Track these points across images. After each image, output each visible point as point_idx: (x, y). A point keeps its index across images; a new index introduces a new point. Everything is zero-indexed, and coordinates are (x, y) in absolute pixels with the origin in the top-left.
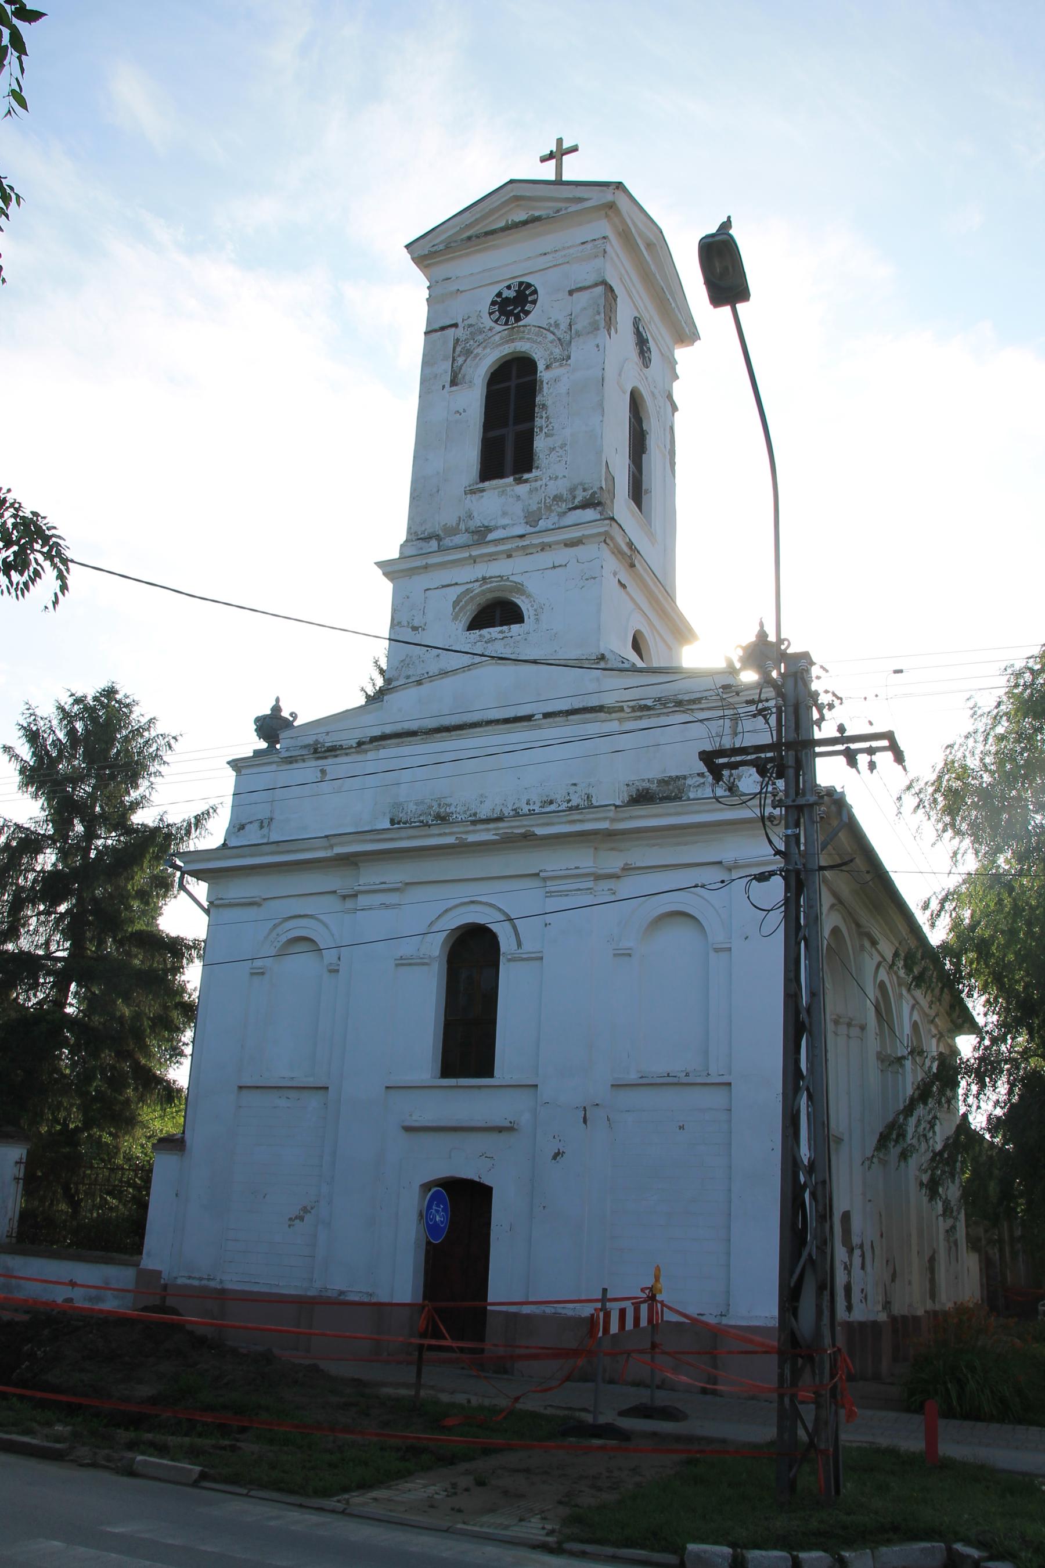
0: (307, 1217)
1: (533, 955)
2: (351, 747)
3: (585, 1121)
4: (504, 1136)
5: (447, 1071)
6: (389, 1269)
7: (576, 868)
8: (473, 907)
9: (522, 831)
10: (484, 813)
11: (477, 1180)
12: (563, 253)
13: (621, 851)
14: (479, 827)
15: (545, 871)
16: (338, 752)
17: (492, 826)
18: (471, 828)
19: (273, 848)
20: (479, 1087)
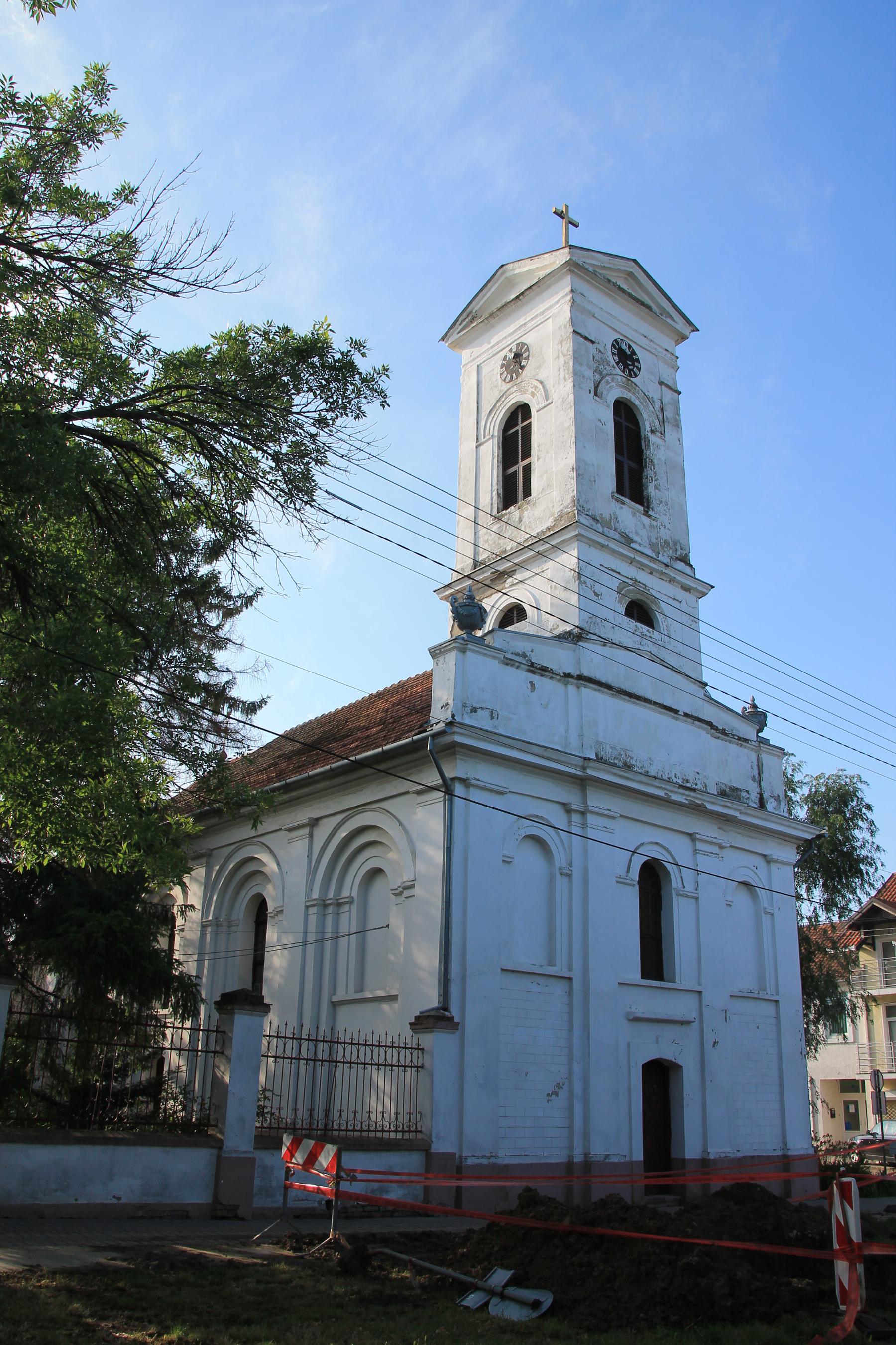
0: (561, 1092)
2: (559, 675)
4: (684, 1027)
6: (618, 1136)
10: (652, 772)
12: (654, 346)
14: (681, 791)
16: (547, 674)
17: (687, 792)
18: (676, 789)
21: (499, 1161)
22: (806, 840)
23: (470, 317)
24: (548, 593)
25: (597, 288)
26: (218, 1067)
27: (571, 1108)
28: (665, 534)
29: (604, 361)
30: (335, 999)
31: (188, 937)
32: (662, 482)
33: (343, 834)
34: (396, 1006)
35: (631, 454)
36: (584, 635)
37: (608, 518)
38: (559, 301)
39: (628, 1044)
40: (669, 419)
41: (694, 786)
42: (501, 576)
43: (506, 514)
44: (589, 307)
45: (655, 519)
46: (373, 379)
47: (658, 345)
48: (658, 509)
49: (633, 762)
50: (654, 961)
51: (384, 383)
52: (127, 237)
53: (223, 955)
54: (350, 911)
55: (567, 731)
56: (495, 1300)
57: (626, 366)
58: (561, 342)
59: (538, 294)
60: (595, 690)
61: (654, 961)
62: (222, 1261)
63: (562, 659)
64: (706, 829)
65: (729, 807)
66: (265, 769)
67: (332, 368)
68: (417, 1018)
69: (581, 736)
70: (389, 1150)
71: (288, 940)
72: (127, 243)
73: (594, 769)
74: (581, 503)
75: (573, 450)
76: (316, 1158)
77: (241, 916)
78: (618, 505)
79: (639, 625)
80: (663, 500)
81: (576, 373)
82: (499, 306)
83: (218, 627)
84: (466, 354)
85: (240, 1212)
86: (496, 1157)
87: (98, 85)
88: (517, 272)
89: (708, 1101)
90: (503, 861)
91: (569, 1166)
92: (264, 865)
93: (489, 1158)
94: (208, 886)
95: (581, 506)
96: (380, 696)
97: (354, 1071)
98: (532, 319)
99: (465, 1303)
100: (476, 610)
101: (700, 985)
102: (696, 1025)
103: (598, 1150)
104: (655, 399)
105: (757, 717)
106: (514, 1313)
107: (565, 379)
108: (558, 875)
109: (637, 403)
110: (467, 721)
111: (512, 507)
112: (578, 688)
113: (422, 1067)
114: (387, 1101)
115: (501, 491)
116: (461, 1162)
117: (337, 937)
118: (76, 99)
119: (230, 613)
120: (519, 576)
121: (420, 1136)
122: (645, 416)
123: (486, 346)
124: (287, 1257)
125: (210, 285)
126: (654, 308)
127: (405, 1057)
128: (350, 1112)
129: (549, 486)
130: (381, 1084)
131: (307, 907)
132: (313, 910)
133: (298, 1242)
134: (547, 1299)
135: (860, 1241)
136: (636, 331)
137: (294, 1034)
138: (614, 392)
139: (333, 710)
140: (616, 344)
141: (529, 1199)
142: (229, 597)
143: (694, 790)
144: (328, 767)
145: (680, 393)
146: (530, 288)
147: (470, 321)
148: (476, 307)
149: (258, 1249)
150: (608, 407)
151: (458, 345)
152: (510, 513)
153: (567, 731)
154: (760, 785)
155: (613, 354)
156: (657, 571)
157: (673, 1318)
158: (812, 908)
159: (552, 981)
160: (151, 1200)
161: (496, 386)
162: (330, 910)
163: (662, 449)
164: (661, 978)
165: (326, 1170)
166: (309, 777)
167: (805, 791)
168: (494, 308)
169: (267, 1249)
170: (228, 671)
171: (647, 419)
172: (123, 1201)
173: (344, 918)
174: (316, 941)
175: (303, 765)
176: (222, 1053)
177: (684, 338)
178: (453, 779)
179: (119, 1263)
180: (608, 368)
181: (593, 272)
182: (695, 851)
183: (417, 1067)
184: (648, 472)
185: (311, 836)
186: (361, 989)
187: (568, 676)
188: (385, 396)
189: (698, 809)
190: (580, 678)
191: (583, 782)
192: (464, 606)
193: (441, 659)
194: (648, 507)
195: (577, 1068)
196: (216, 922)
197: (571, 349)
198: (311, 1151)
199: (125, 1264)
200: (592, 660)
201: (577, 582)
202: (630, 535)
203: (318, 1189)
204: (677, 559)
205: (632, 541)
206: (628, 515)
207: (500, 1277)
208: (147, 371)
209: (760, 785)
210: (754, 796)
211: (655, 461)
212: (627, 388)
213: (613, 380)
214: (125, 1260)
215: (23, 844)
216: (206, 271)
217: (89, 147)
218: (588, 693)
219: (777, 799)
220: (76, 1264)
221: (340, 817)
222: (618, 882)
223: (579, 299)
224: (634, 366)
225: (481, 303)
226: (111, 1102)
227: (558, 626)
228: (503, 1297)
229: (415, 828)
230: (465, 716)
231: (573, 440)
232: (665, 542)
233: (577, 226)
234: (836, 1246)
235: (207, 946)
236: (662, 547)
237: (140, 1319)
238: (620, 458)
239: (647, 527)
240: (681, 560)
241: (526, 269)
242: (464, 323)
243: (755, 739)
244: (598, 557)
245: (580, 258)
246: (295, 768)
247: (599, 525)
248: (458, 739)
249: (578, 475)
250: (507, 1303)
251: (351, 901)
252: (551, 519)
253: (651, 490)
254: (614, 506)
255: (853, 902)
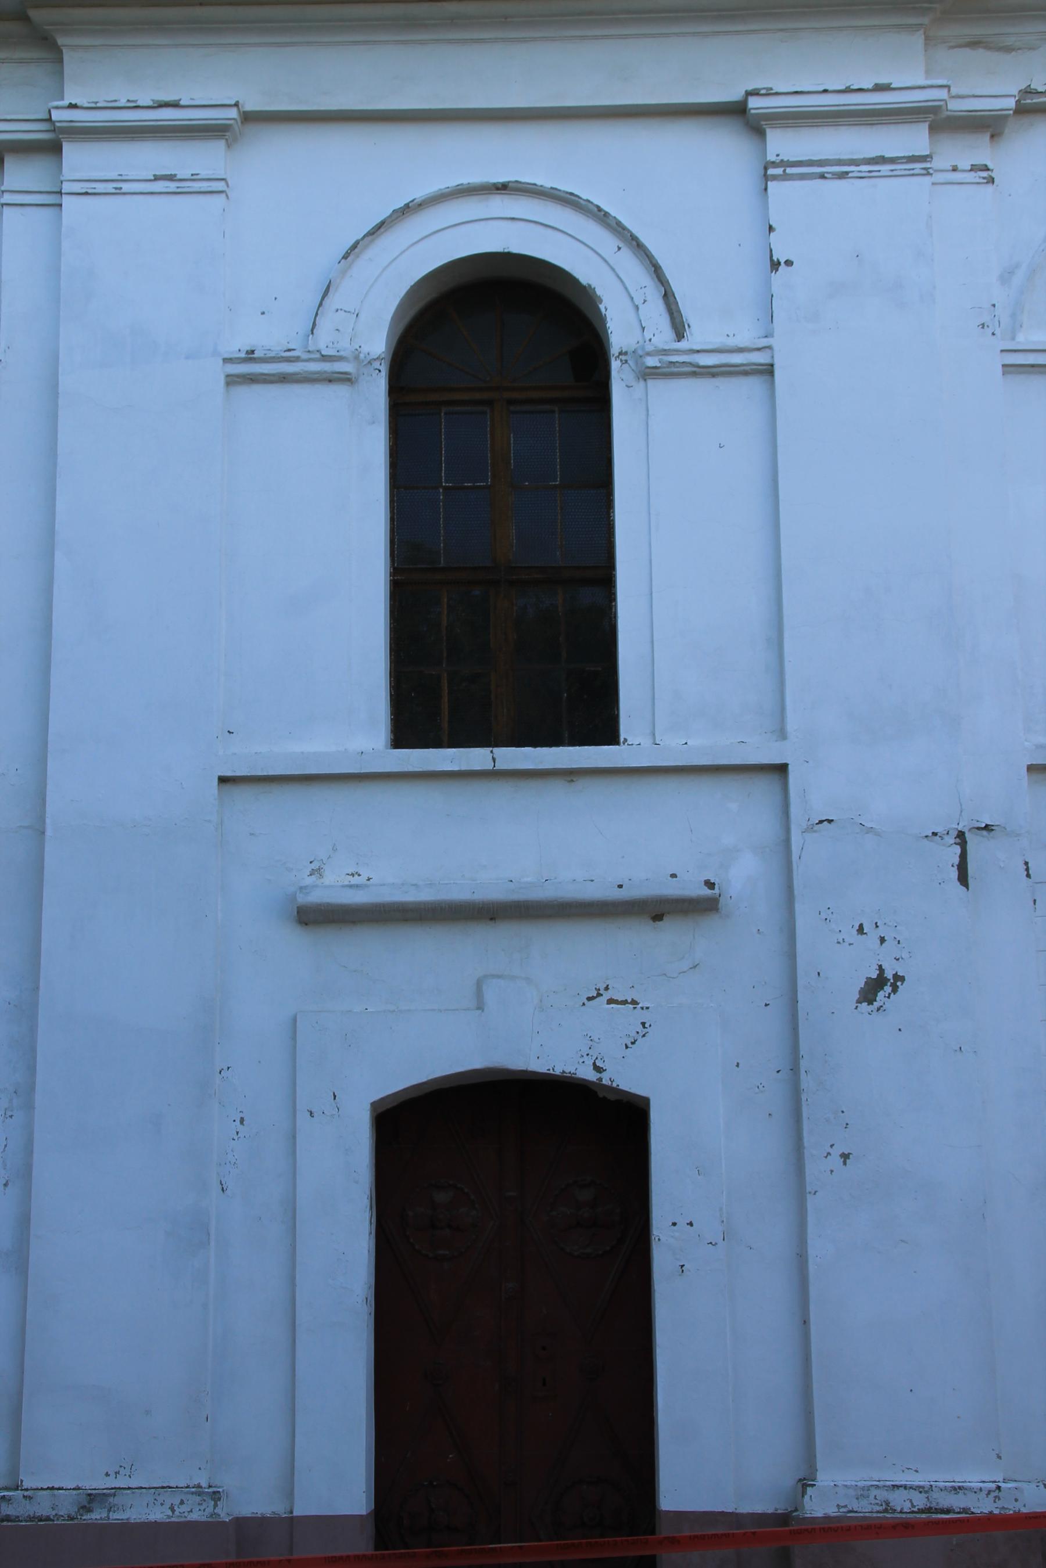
1: (737, 359)
3: (963, 878)
4: (670, 935)
5: (411, 726)
7: (879, 88)
8: (499, 205)
11: (590, 1075)
13: (1008, 49)
15: (770, 93)
20: (571, 774)
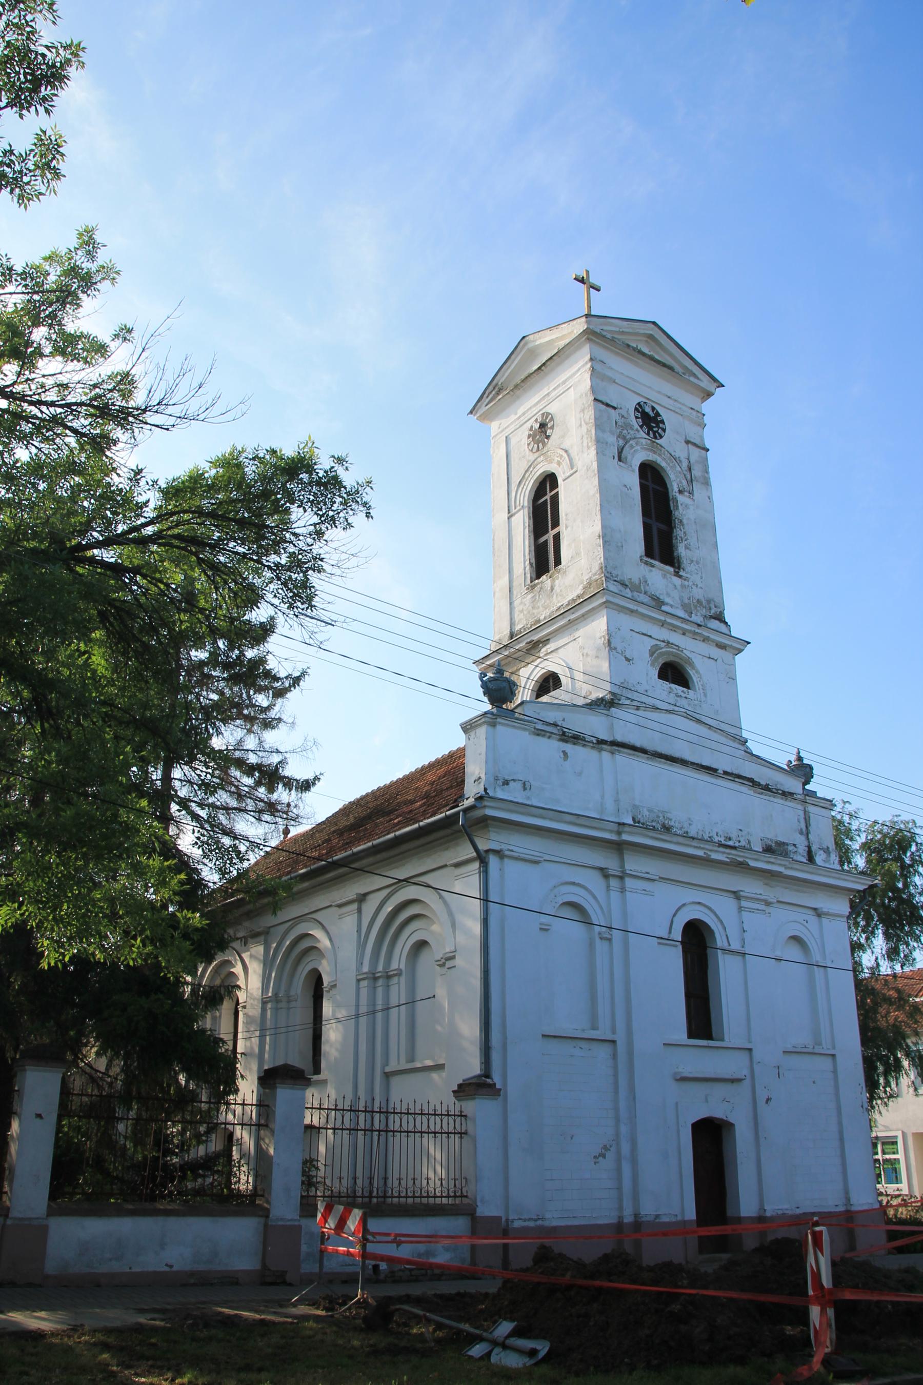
0: (608, 1154)
6: (669, 1194)
9: (741, 859)
10: (692, 833)
14: (721, 849)
17: (728, 851)
18: (716, 848)
19: (573, 819)
21: (546, 1223)
22: (859, 891)
23: (496, 390)
24: (581, 660)
25: (617, 354)
26: (263, 1140)
27: (619, 1170)
28: (698, 593)
29: (628, 426)
30: (387, 1069)
31: (250, 1014)
32: (693, 541)
33: (388, 908)
34: (444, 1074)
35: (660, 517)
36: (616, 701)
37: (637, 582)
38: (579, 369)
39: (677, 1103)
40: (698, 477)
41: (737, 844)
42: (535, 647)
43: (538, 584)
44: (609, 373)
45: (686, 579)
46: (357, 492)
47: (683, 404)
48: (689, 569)
49: (672, 823)
50: (701, 1019)
51: (368, 495)
52: (128, 374)
53: (283, 1030)
54: (399, 983)
55: (603, 797)
56: (497, 1350)
57: (650, 428)
58: (583, 411)
59: (559, 364)
60: (630, 755)
61: (701, 1019)
62: (254, 1320)
63: (595, 725)
64: (751, 887)
65: (773, 863)
66: (319, 845)
67: (319, 483)
68: (460, 1086)
69: (617, 801)
70: (433, 1215)
71: (342, 1013)
72: (125, 382)
73: (630, 833)
74: (609, 569)
75: (599, 517)
76: (345, 1223)
77: (299, 991)
78: (648, 568)
79: (674, 686)
80: (694, 559)
81: (598, 441)
82: (523, 377)
83: (269, 708)
84: (495, 426)
85: (288, 1278)
86: (543, 1219)
87: (88, 242)
88: (538, 343)
89: (762, 1159)
90: (541, 929)
91: (619, 1227)
92: (318, 941)
93: (536, 1220)
94: (267, 963)
95: (609, 573)
96: (431, 766)
97: (411, 1139)
98: (555, 389)
99: (470, 1353)
100: (505, 684)
101: (750, 1042)
102: (747, 1082)
103: (648, 1210)
104: (682, 458)
105: (803, 771)
106: (512, 1361)
107: (588, 448)
108: (598, 940)
109: (663, 464)
110: (500, 794)
111: (544, 577)
112: (613, 753)
113: (466, 1133)
114: (438, 1168)
115: (533, 561)
116: (508, 1225)
117: (388, 1009)
118: (70, 259)
119: (280, 693)
120: (551, 646)
121: (465, 1201)
122: (672, 476)
123: (513, 417)
124: (319, 1316)
125: (201, 417)
126: (677, 367)
127: (448, 1124)
128: (366, 1179)
129: (578, 554)
130: (432, 1151)
131: (358, 981)
132: (364, 983)
133: (331, 1303)
134: (543, 1347)
135: (831, 1286)
136: (659, 392)
137: (336, 1105)
138: (639, 456)
139: (388, 783)
140: (639, 408)
141: (544, 1256)
142: (276, 679)
143: (734, 848)
144: (370, 844)
145: (708, 450)
146: (551, 358)
147: (497, 393)
148: (501, 379)
149: (294, 1309)
150: (633, 471)
151: (486, 417)
152: (542, 582)
153: (603, 797)
154: (808, 838)
155: (637, 418)
156: (690, 631)
157: (655, 1362)
158: (874, 958)
159: (594, 1046)
160: (201, 1267)
161: (524, 457)
162: (380, 982)
163: (692, 508)
164: (709, 1037)
165: (354, 1233)
166: (354, 854)
167: (862, 839)
168: (518, 380)
169: (303, 1310)
170: (278, 751)
171: (675, 480)
172: (175, 1269)
173: (394, 990)
174: (368, 1014)
175: (351, 842)
176: (267, 1126)
177: (709, 395)
178: (487, 851)
179: (158, 1323)
180: (632, 432)
181: (609, 338)
182: (740, 908)
183: (461, 1133)
184: (678, 532)
185: (359, 911)
186: (412, 1060)
187: (601, 742)
188: (369, 508)
189: (741, 867)
190: (614, 743)
191: (619, 847)
192: (491, 680)
193: (472, 734)
194: (679, 568)
195: (624, 1129)
196: (276, 998)
197: (593, 417)
198: (341, 1217)
199: (162, 1323)
200: (624, 724)
201: (607, 649)
202: (661, 597)
203: (348, 1251)
204: (711, 617)
205: (663, 603)
206: (658, 577)
207: (505, 1328)
208: (151, 499)
209: (808, 838)
210: (802, 849)
211: (685, 521)
212: (651, 451)
213: (637, 444)
214: (162, 1320)
215: (45, 944)
216: (193, 407)
217: (89, 295)
218: (623, 759)
219: (827, 851)
220: (118, 1324)
221: (385, 893)
222: (659, 943)
223: (598, 367)
224: (659, 427)
225: (506, 375)
226: (161, 1176)
227: (591, 693)
228: (505, 1347)
229: (453, 902)
230: (498, 789)
231: (598, 508)
232: (698, 601)
233: (598, 290)
234: (811, 1292)
235: (268, 1023)
236: (696, 607)
237: (161, 1368)
238: (648, 521)
239: (679, 587)
240: (715, 618)
241: (547, 339)
242: (491, 396)
243: (801, 792)
244: (627, 622)
245: (597, 326)
246: (343, 845)
247: (628, 590)
248: (489, 812)
249: (605, 542)
250: (508, 1352)
251: (399, 974)
252: (581, 587)
253: (681, 550)
254: (644, 570)
255: (917, 950)
